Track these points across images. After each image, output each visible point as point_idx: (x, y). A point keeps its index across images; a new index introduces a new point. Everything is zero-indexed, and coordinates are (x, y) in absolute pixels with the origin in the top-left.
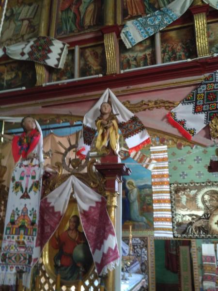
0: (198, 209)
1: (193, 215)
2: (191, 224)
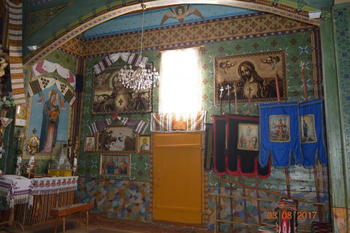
0: (109, 89)
1: (105, 95)
2: (103, 102)
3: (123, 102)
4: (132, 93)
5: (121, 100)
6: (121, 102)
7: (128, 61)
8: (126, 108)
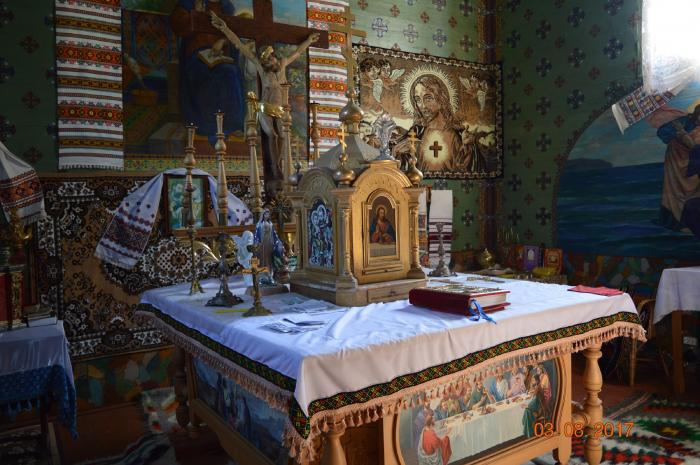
0: (403, 114)
3: (440, 148)
4: (462, 130)
5: (436, 143)
6: (436, 148)
7: (450, 224)
8: (449, 167)
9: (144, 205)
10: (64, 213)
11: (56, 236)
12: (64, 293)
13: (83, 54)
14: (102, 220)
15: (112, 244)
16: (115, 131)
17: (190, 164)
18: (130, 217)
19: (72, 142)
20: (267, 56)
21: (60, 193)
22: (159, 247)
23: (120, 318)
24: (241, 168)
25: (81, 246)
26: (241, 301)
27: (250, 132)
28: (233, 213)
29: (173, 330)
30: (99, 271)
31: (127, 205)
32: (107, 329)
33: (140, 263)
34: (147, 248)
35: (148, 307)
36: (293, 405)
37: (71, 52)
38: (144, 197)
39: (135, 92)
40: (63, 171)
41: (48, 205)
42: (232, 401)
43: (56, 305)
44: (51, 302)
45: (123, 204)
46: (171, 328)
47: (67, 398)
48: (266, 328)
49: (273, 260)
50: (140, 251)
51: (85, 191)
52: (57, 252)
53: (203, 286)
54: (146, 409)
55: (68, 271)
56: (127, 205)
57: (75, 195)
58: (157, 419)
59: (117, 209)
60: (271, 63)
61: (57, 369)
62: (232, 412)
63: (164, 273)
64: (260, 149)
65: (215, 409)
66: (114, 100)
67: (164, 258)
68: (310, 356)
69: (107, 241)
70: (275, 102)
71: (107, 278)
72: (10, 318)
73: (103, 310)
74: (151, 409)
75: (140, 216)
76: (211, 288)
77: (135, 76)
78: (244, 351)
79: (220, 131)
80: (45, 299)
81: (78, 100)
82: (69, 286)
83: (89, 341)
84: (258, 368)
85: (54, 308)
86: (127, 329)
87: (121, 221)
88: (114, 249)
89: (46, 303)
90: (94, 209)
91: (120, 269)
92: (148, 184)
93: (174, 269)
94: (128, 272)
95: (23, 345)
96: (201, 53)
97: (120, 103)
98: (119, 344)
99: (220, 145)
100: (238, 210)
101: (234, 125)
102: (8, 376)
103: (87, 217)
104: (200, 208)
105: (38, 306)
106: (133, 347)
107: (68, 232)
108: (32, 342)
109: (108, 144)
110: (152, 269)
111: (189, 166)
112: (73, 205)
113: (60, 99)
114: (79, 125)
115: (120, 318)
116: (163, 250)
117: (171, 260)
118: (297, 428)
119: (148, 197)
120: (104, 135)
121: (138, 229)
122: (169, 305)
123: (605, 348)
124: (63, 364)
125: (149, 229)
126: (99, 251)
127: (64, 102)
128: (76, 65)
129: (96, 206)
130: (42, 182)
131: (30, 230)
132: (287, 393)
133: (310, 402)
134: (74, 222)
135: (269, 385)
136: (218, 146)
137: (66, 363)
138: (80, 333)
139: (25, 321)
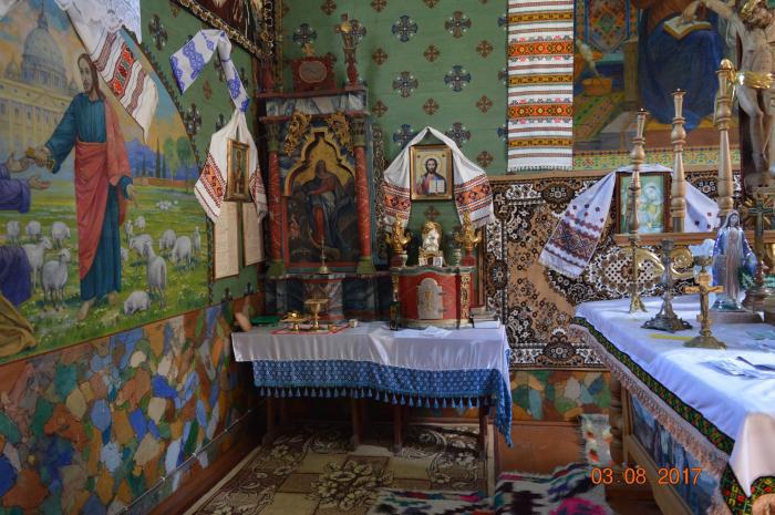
9: (592, 207)
10: (510, 217)
11: (503, 240)
12: (508, 298)
13: (533, 49)
14: (548, 224)
15: (558, 250)
16: (564, 127)
17: (638, 158)
18: (577, 221)
19: (520, 143)
20: (751, 9)
21: (507, 196)
22: (608, 256)
23: (562, 330)
24: (703, 161)
25: (526, 251)
26: (689, 327)
27: (720, 112)
28: (703, 217)
29: (606, 352)
30: (543, 277)
31: (575, 208)
32: (549, 341)
33: (586, 272)
34: (595, 255)
35: (582, 321)
36: (729, 477)
37: (522, 50)
38: (593, 199)
39: (587, 82)
40: (512, 173)
41: (497, 207)
42: (670, 450)
43: (501, 309)
44: (497, 305)
45: (570, 206)
46: (603, 348)
47: (503, 404)
48: (709, 365)
49: (740, 276)
50: (586, 259)
51: (532, 193)
52: (503, 256)
53: (646, 304)
54: (584, 433)
55: (513, 276)
56: (575, 208)
57: (522, 197)
58: (595, 448)
59: (564, 212)
60: (757, 17)
61: (495, 373)
62: (669, 462)
63: (612, 286)
64: (737, 135)
65: (651, 452)
66: (564, 94)
67: (613, 269)
68: (759, 414)
69: (551, 247)
70: (760, 68)
71: (551, 286)
72: (459, 317)
73: (545, 320)
74: (590, 434)
75: (587, 220)
76: (654, 306)
77: (587, 64)
78: (676, 389)
79: (678, 114)
80: (492, 303)
81: (527, 98)
82: (513, 291)
83: (530, 350)
84: (691, 414)
85: (499, 312)
86: (570, 343)
87: (566, 226)
88: (558, 255)
89: (492, 306)
90: (540, 213)
91: (565, 277)
92: (597, 185)
93: (625, 281)
94: (573, 282)
95: (466, 344)
96: (667, 23)
97: (570, 97)
98: (559, 358)
99: (678, 132)
100: (709, 214)
101: (700, 106)
102: (453, 372)
103: (533, 221)
104: (659, 212)
105: (483, 308)
106: (575, 363)
107: (514, 236)
108: (473, 343)
109: (536, 142)
110: (600, 281)
111: (636, 161)
112: (520, 208)
113: (511, 99)
114: (528, 124)
115: (562, 330)
116: (612, 258)
117: (622, 272)
118: (730, 506)
119: (597, 199)
120: (552, 133)
121: (585, 235)
122: (602, 322)
123: (608, 499)
124: (500, 369)
125: (597, 234)
126: (544, 257)
127: (515, 102)
128: (527, 62)
129: (542, 209)
130: (493, 185)
131: (480, 233)
132: (722, 454)
133: (757, 475)
134: (520, 225)
135: (702, 439)
136: (674, 134)
137: (505, 371)
138: (521, 340)
139: (471, 321)
